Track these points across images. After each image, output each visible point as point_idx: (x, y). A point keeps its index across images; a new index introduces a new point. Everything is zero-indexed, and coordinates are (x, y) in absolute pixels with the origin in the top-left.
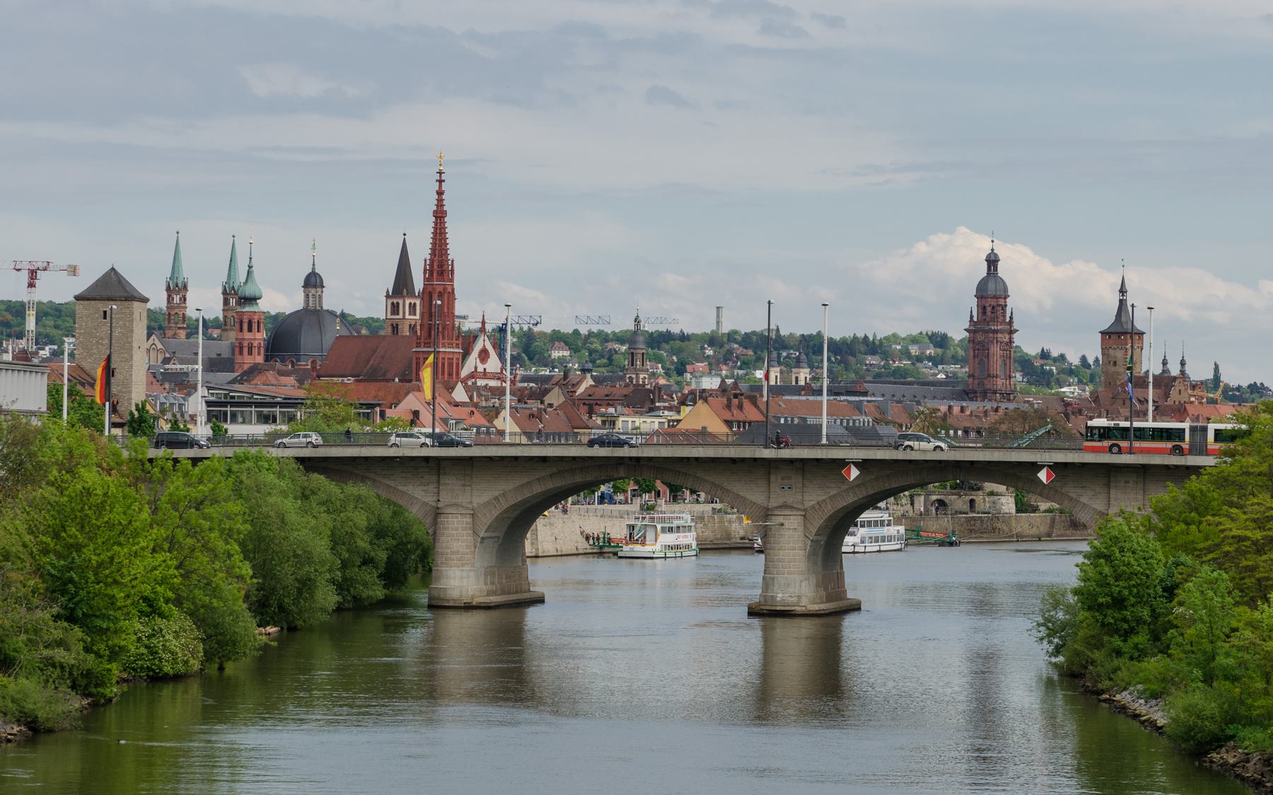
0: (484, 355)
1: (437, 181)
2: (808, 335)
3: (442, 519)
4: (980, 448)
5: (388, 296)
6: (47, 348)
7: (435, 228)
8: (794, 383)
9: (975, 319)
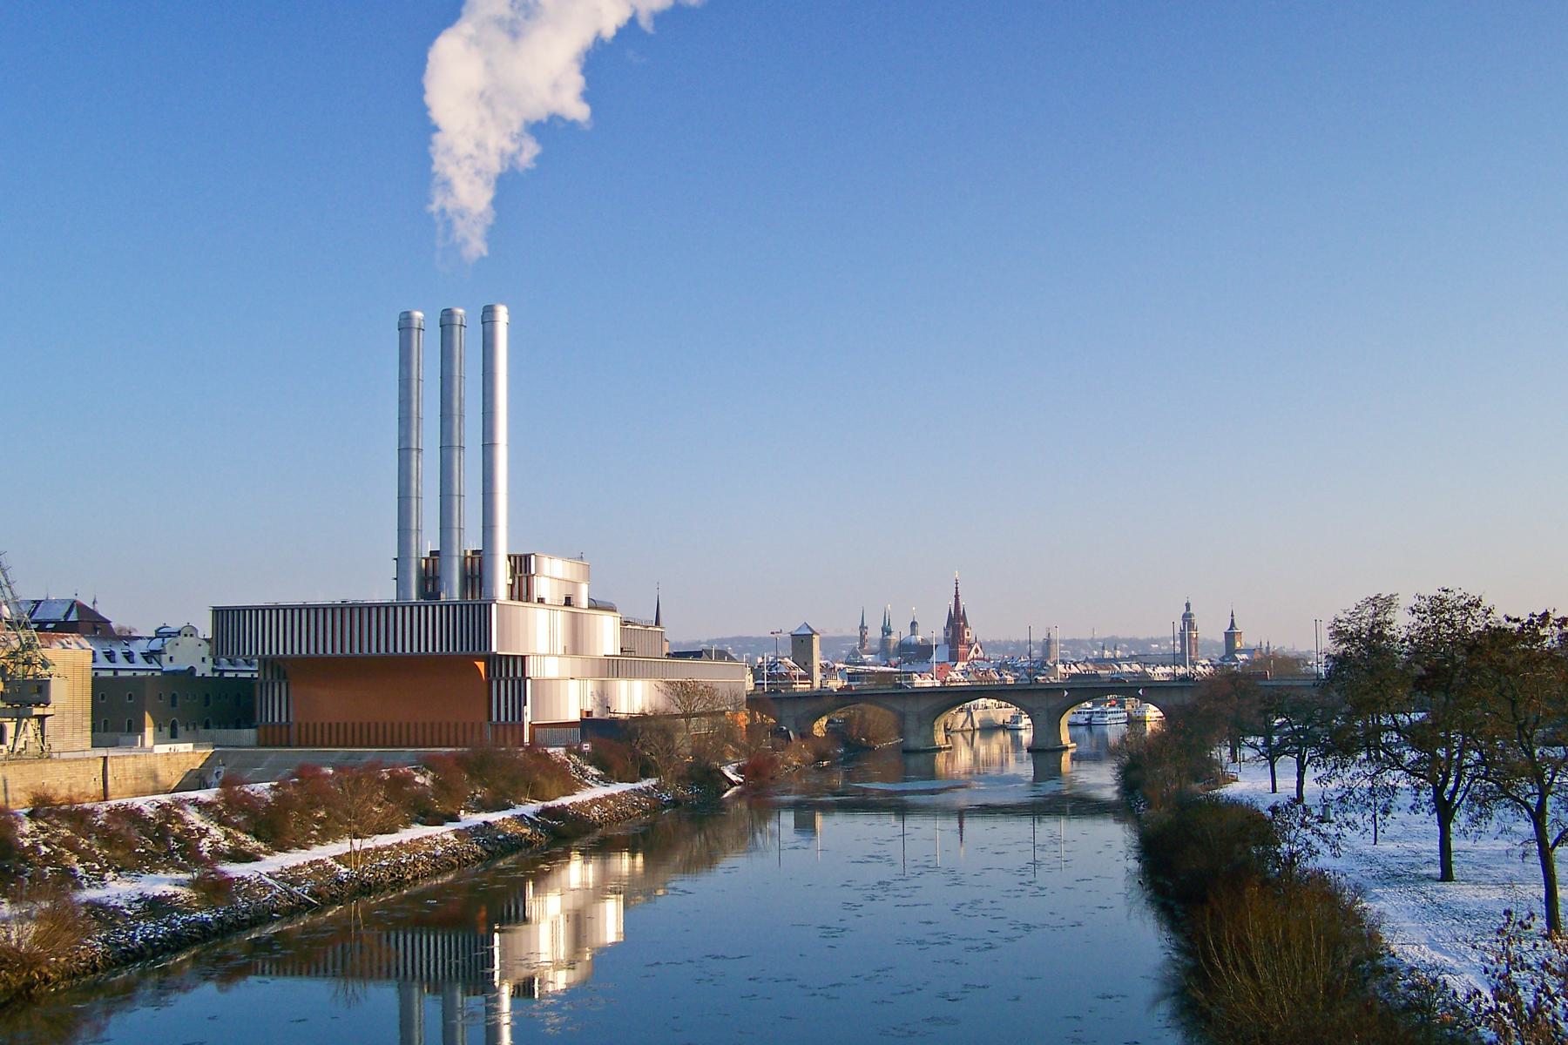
0: (977, 651)
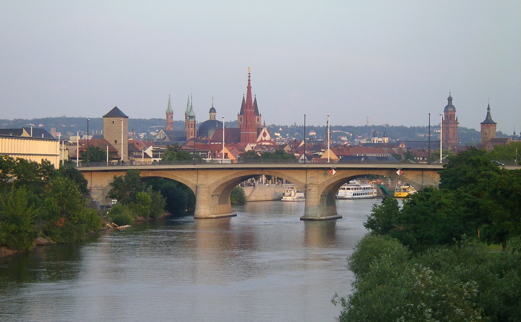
0: (265, 135)
1: (248, 76)
2: (398, 127)
3: (198, 189)
4: (415, 163)
5: (238, 115)
6: (143, 134)
7: (248, 92)
8: (373, 142)
9: (444, 120)
